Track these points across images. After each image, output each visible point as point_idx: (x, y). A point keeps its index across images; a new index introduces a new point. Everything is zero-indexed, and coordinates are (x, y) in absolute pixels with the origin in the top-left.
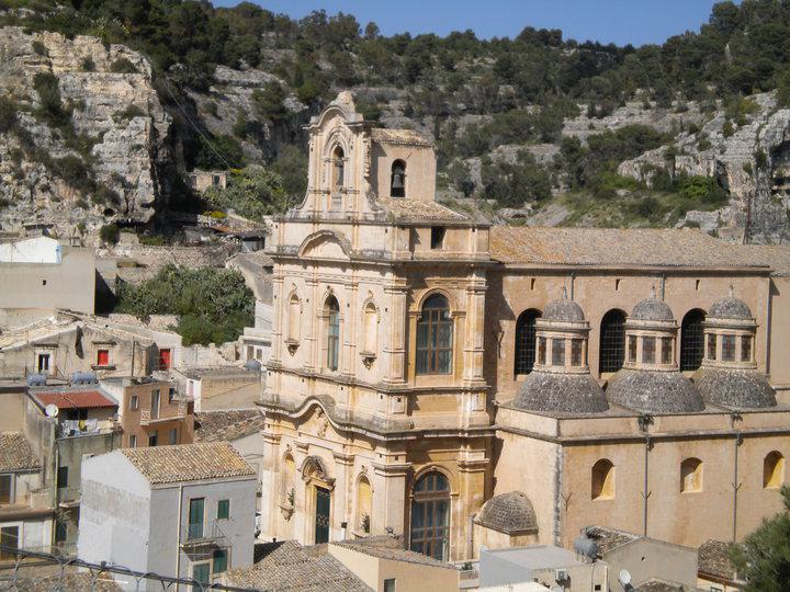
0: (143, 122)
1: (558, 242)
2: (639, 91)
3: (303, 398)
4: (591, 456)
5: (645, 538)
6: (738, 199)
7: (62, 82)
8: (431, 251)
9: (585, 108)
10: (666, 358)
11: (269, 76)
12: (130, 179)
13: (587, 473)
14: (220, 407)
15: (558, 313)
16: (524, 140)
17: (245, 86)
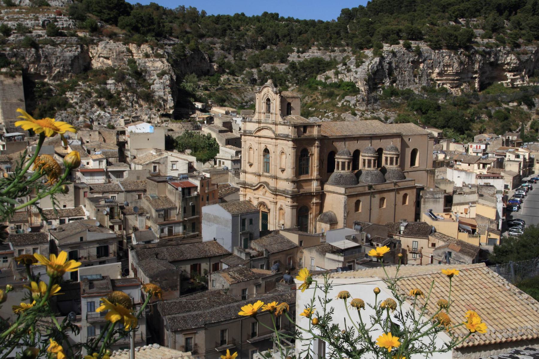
0: (167, 77)
2: (315, 43)
3: (257, 183)
4: (354, 200)
7: (138, 62)
9: (295, 49)
12: (165, 98)
16: (274, 62)
17: (170, 45)
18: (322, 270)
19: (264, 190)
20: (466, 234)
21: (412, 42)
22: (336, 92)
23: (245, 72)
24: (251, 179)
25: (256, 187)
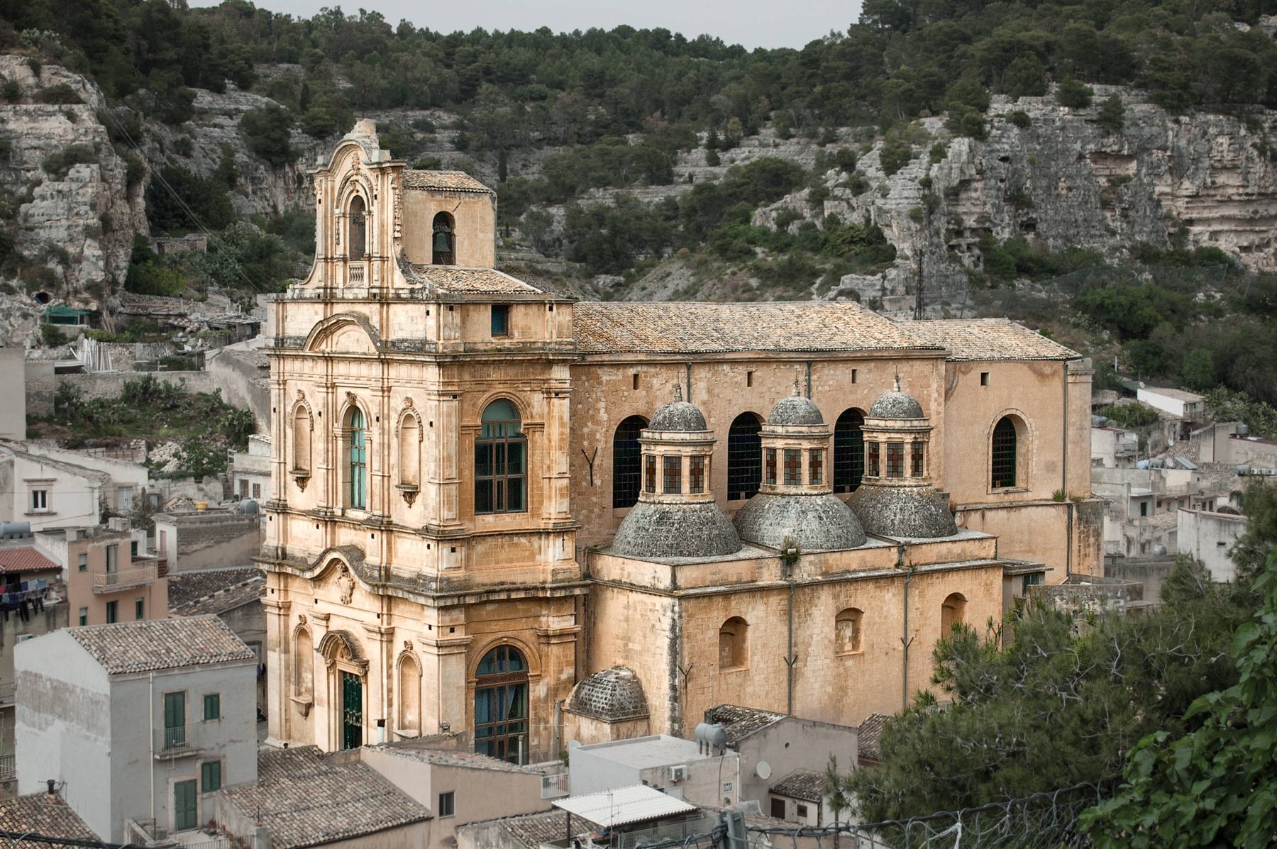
1: (668, 322)
5: (790, 716)
6: (907, 258)
8: (493, 340)
10: (815, 477)
11: (266, 99)
12: (71, 250)
13: (712, 635)
14: (204, 566)
15: (669, 424)
19: (345, 581)
21: (1096, 88)
22: (816, 261)
25: (317, 571)
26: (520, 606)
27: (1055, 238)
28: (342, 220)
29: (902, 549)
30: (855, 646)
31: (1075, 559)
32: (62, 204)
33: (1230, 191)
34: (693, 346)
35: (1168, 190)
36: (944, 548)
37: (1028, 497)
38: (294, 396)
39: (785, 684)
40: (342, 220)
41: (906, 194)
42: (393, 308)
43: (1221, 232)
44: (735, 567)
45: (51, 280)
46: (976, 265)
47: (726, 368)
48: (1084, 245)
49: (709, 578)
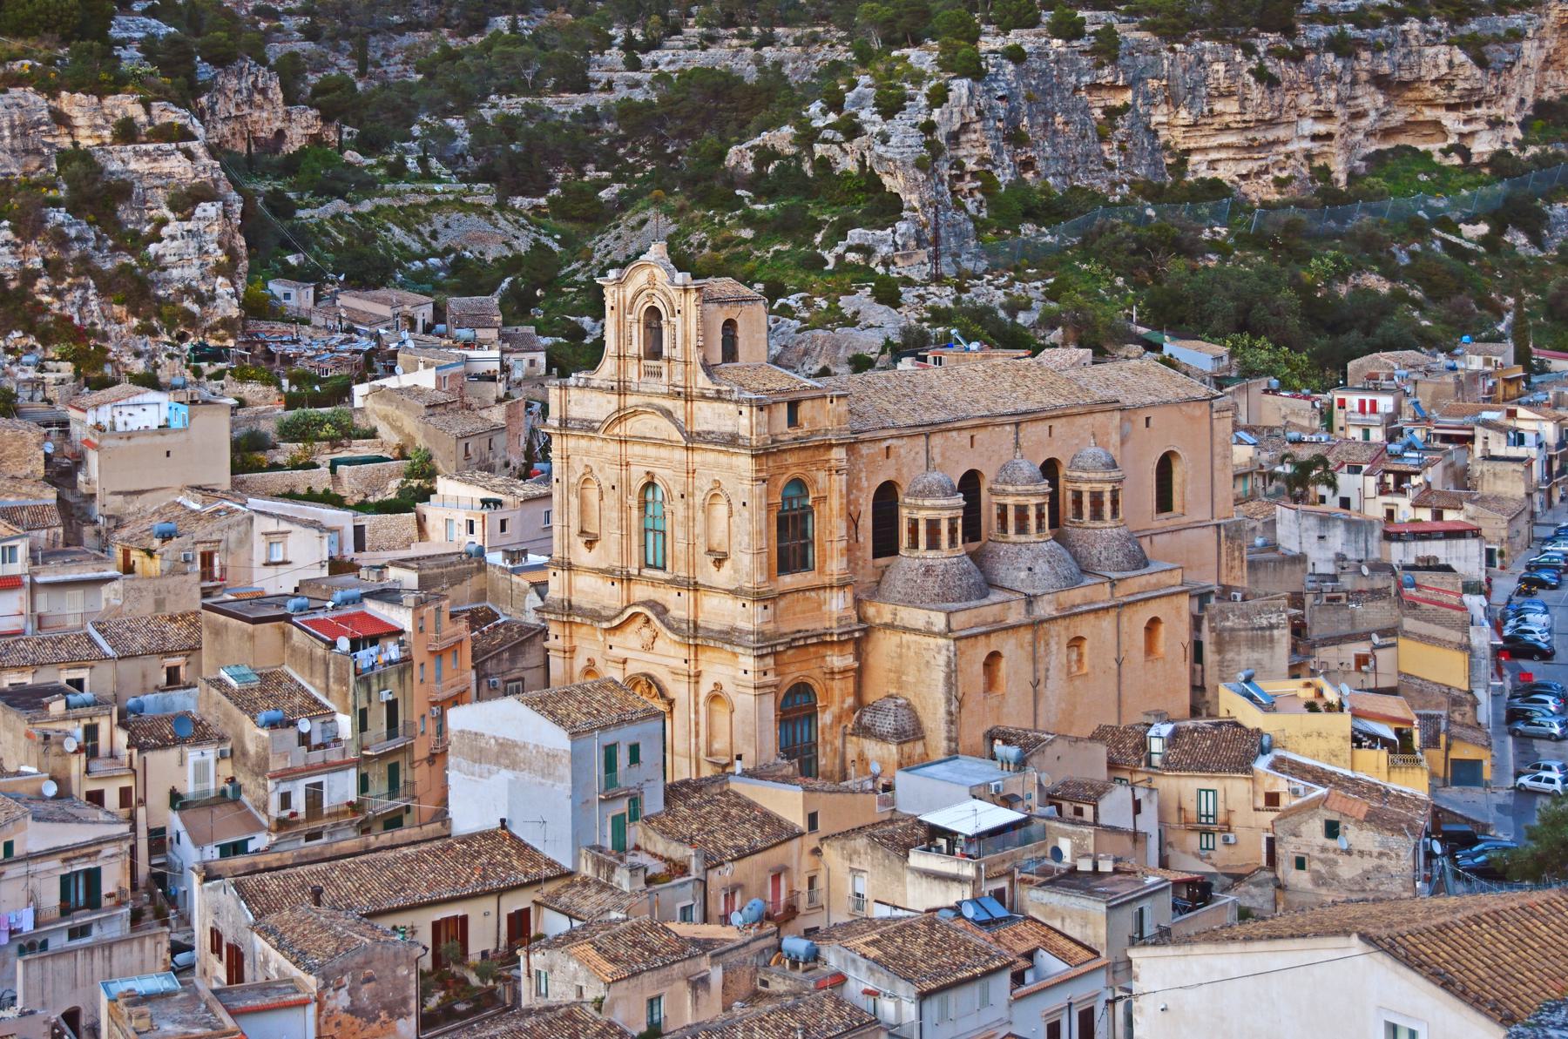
3: (619, 606)
6: (915, 210)
18: (900, 913)
20: (1382, 755)
23: (416, 130)
24: (591, 590)
25: (616, 622)
26: (812, 649)
27: (1054, 175)
28: (635, 326)
29: (1113, 583)
30: (1080, 668)
31: (1224, 572)
32: (193, 244)
33: (1227, 119)
34: (927, 418)
35: (1164, 119)
36: (1143, 580)
37: (1185, 520)
38: (580, 470)
39: (1031, 704)
40: (635, 326)
41: (909, 141)
42: (696, 404)
43: (1219, 160)
44: (989, 609)
45: (191, 319)
46: (979, 211)
47: (954, 434)
48: (1083, 182)
49: (974, 620)
